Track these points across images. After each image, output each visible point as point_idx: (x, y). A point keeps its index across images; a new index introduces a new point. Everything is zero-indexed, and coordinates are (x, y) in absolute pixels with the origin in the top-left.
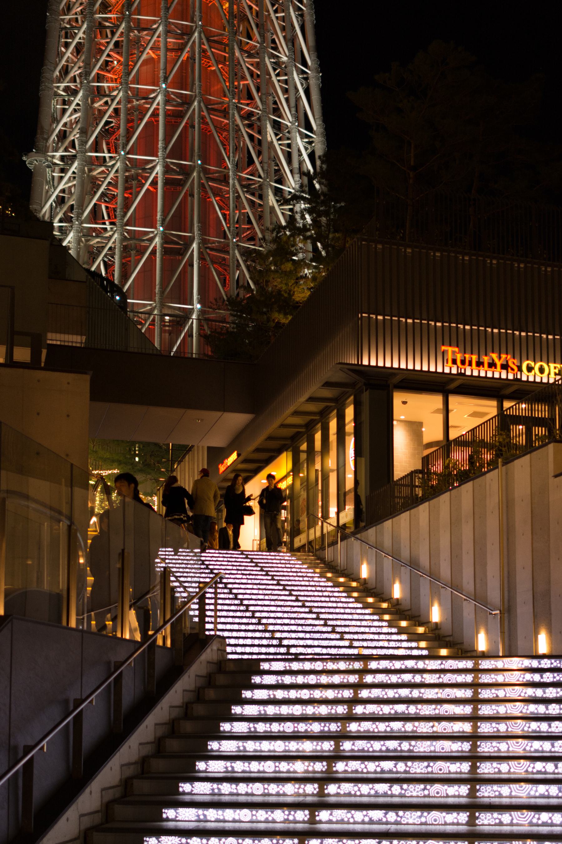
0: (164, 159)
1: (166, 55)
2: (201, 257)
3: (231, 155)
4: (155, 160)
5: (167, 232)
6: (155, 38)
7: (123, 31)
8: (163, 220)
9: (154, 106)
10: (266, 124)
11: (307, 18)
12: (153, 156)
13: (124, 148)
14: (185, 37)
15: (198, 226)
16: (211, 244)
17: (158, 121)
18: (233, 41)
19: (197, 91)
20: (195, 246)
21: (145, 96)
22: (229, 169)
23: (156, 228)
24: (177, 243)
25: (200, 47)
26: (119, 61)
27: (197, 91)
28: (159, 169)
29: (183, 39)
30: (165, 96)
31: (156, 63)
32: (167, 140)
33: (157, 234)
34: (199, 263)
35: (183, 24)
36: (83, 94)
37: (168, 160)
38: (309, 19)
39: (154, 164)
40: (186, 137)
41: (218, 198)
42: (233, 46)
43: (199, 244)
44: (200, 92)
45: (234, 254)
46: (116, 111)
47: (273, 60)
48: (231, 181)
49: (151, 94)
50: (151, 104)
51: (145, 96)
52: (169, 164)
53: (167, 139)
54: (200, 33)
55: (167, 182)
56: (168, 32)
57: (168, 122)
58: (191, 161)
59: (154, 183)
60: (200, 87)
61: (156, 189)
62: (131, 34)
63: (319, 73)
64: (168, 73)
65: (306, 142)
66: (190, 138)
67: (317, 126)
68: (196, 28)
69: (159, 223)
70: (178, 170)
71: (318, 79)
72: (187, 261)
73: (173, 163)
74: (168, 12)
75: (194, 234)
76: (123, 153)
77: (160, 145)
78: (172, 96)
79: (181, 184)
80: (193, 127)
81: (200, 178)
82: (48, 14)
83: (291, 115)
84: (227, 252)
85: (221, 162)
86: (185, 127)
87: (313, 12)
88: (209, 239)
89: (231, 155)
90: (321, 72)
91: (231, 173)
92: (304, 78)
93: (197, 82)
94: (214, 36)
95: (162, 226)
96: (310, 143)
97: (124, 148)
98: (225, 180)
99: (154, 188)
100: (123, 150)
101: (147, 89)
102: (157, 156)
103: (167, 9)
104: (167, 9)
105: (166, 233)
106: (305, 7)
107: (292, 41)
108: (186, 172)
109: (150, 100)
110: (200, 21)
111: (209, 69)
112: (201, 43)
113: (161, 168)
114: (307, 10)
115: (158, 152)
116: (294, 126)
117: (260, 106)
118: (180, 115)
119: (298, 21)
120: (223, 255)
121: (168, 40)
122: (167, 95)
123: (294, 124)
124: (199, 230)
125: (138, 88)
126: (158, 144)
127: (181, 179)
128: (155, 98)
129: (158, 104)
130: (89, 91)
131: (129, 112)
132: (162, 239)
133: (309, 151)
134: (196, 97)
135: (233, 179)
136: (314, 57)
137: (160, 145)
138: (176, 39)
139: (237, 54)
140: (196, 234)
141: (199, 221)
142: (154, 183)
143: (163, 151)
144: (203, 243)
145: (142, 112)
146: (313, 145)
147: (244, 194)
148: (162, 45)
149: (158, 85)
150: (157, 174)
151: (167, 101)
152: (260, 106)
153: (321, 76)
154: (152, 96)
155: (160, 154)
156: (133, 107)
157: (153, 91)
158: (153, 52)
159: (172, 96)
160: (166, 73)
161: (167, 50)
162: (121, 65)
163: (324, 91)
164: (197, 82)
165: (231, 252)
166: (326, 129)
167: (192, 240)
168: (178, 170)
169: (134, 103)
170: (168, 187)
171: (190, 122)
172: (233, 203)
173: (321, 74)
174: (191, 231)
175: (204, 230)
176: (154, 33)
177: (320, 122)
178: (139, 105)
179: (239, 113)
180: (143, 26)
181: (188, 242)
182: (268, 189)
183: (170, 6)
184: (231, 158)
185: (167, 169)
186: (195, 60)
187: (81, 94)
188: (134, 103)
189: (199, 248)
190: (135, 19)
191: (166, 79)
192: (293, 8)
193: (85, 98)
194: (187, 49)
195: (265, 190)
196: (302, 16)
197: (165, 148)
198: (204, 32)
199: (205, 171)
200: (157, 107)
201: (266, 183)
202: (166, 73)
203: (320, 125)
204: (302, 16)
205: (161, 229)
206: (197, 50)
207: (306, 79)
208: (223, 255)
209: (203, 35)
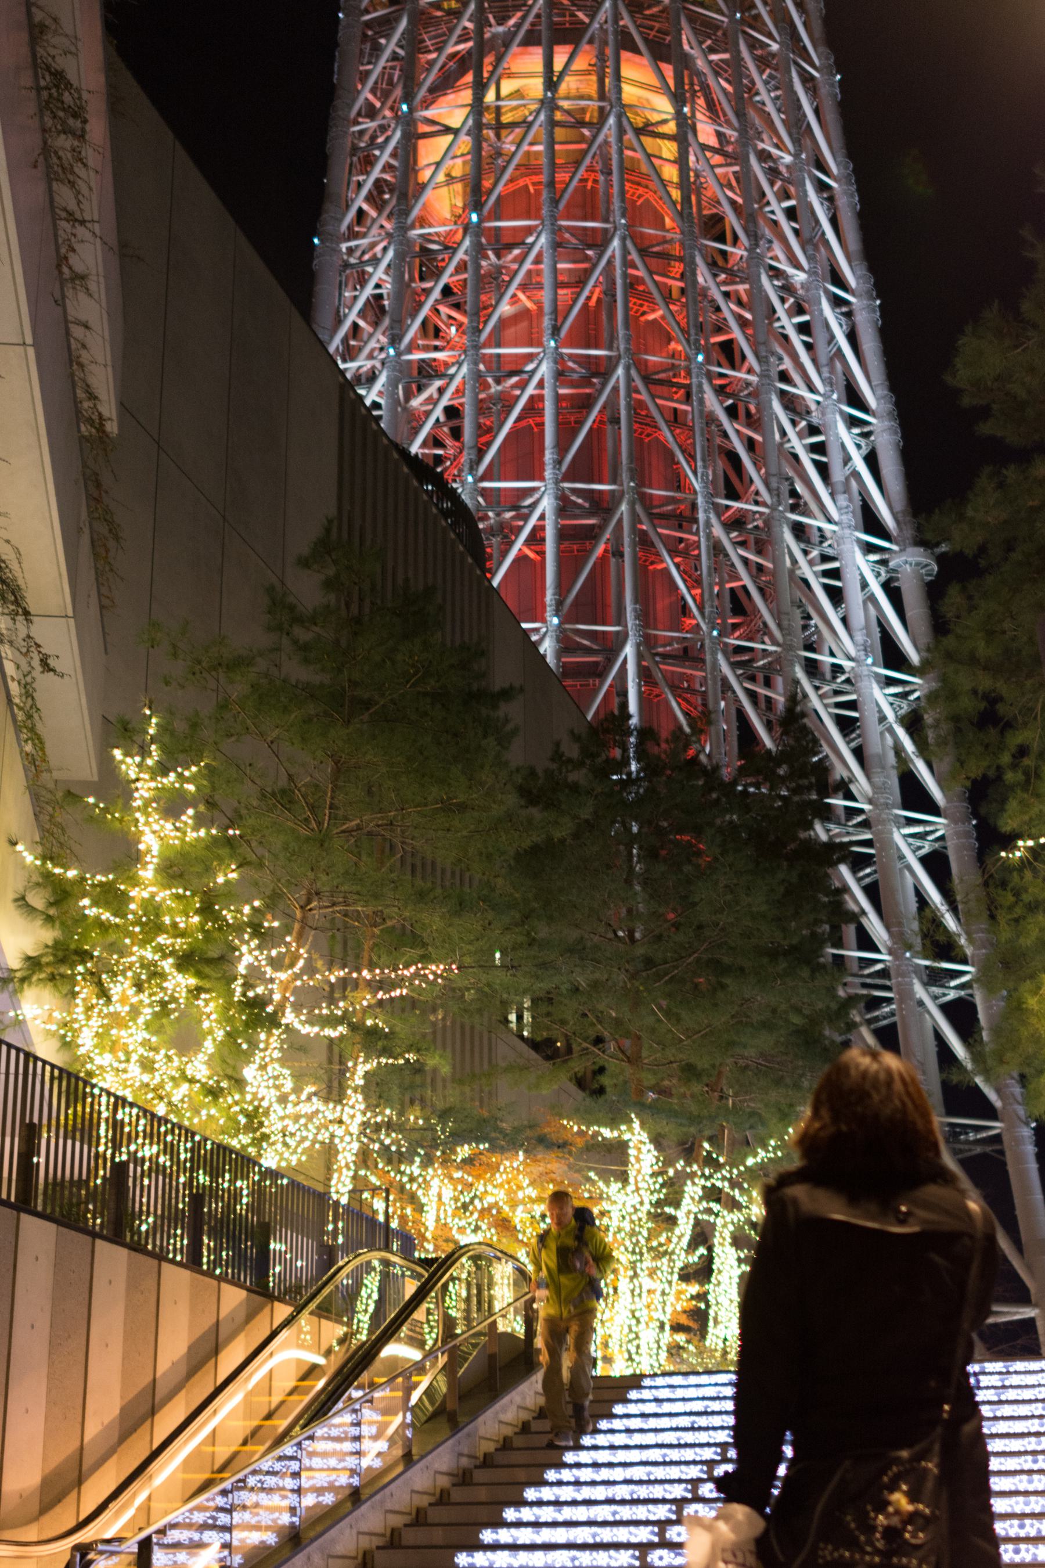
0: (557, 482)
1: (556, 294)
2: (644, 674)
3: (699, 463)
4: (538, 488)
5: (568, 626)
6: (528, 265)
7: (466, 258)
8: (559, 604)
9: (531, 390)
10: (770, 401)
11: (842, 201)
12: (532, 479)
13: (472, 470)
14: (595, 380)
15: (635, 610)
16: (665, 646)
17: (542, 424)
18: (692, 247)
19: (622, 347)
20: (629, 650)
21: (515, 368)
22: (695, 492)
23: (543, 620)
24: (588, 651)
25: (628, 395)
26: (459, 326)
27: (622, 347)
28: (547, 504)
29: (591, 384)
30: (556, 362)
31: (538, 566)
32: (562, 447)
33: (545, 634)
34: (639, 686)
35: (585, 229)
36: (388, 377)
37: (566, 485)
38: (847, 202)
39: (536, 496)
40: (602, 449)
41: (678, 560)
42: (693, 257)
43: (638, 645)
44: (627, 350)
45: (715, 662)
46: (452, 412)
47: (776, 283)
48: (701, 516)
49: (526, 364)
50: (526, 518)
51: (515, 368)
52: (567, 492)
53: (562, 446)
54: (623, 240)
55: (563, 534)
56: (557, 245)
57: (565, 423)
58: (619, 624)
59: (536, 538)
60: (628, 340)
61: (542, 553)
62: (484, 263)
63: (874, 300)
64: (560, 320)
65: (877, 562)
66: (609, 444)
67: (878, 399)
68: (615, 229)
69: (549, 610)
70: (587, 505)
71: (874, 311)
72: (611, 686)
73: (574, 491)
74: (556, 207)
75: (626, 626)
76: (470, 479)
77: (549, 456)
78: (570, 364)
79: (591, 535)
80: (616, 421)
81: (635, 519)
82: (316, 241)
83: (823, 380)
84: (735, 1124)
85: (678, 482)
86: (600, 422)
87: (854, 188)
88: (655, 636)
89: (699, 463)
90: (878, 297)
91: (700, 500)
92: (845, 314)
93: (621, 332)
94: (658, 373)
95: (557, 615)
96: (866, 435)
97: (472, 470)
98: (685, 519)
99: (537, 553)
100: (471, 473)
101: (516, 355)
102: (542, 479)
103: (555, 202)
104: (555, 202)
105: (565, 630)
106: (835, 180)
107: (812, 241)
108: (603, 506)
109: (526, 511)
110: (623, 216)
111: (642, 319)
112: (628, 264)
113: (552, 500)
114: (840, 185)
115: (544, 470)
116: (829, 402)
117: (756, 367)
118: (585, 403)
119: (841, 325)
120: (689, 672)
121: (560, 266)
122: (559, 359)
123: (830, 397)
124: (637, 617)
125: (499, 356)
126: (544, 595)
127: (593, 526)
128: (534, 506)
129: (541, 384)
130: (400, 372)
131: (481, 408)
132: (559, 640)
133: (865, 451)
134: (619, 357)
135: (705, 511)
136: (862, 270)
137: (549, 597)
138: (574, 262)
139: (700, 280)
140: (629, 625)
141: (636, 601)
142: (536, 538)
143: (554, 468)
144: (647, 644)
145: (507, 402)
146: (872, 438)
147: (741, 684)
148: (547, 280)
149: (540, 344)
150: (542, 517)
151: (560, 375)
152: (756, 367)
153: (880, 306)
154: (528, 502)
155: (548, 473)
156: (490, 398)
157: (530, 357)
158: (528, 297)
159: (570, 364)
160: (556, 320)
161: (557, 285)
162: (464, 333)
163: (887, 334)
164: (621, 332)
165: (708, 658)
166: (898, 404)
167: (620, 640)
168: (587, 505)
169: (493, 390)
170: (566, 544)
171: (608, 413)
172: (709, 559)
173: (878, 302)
174: (620, 620)
175: (646, 618)
176: (531, 377)
177: (883, 391)
178: (502, 392)
179: (719, 515)
180: (507, 239)
181: (612, 647)
182: (781, 526)
183: (561, 196)
184: (700, 471)
185: (564, 506)
186: (614, 296)
187: (382, 379)
188: (493, 390)
189: (640, 657)
190: (490, 229)
191: (556, 330)
192: (829, 300)
193: (393, 383)
194: (607, 534)
195: (776, 529)
196: (831, 199)
197: (559, 462)
198: (632, 238)
199: (645, 500)
200: (536, 392)
201: (776, 514)
202: (556, 320)
203: (883, 397)
204: (831, 199)
205: (555, 621)
206: (619, 282)
207: (849, 315)
208: (689, 672)
209: (633, 372)
